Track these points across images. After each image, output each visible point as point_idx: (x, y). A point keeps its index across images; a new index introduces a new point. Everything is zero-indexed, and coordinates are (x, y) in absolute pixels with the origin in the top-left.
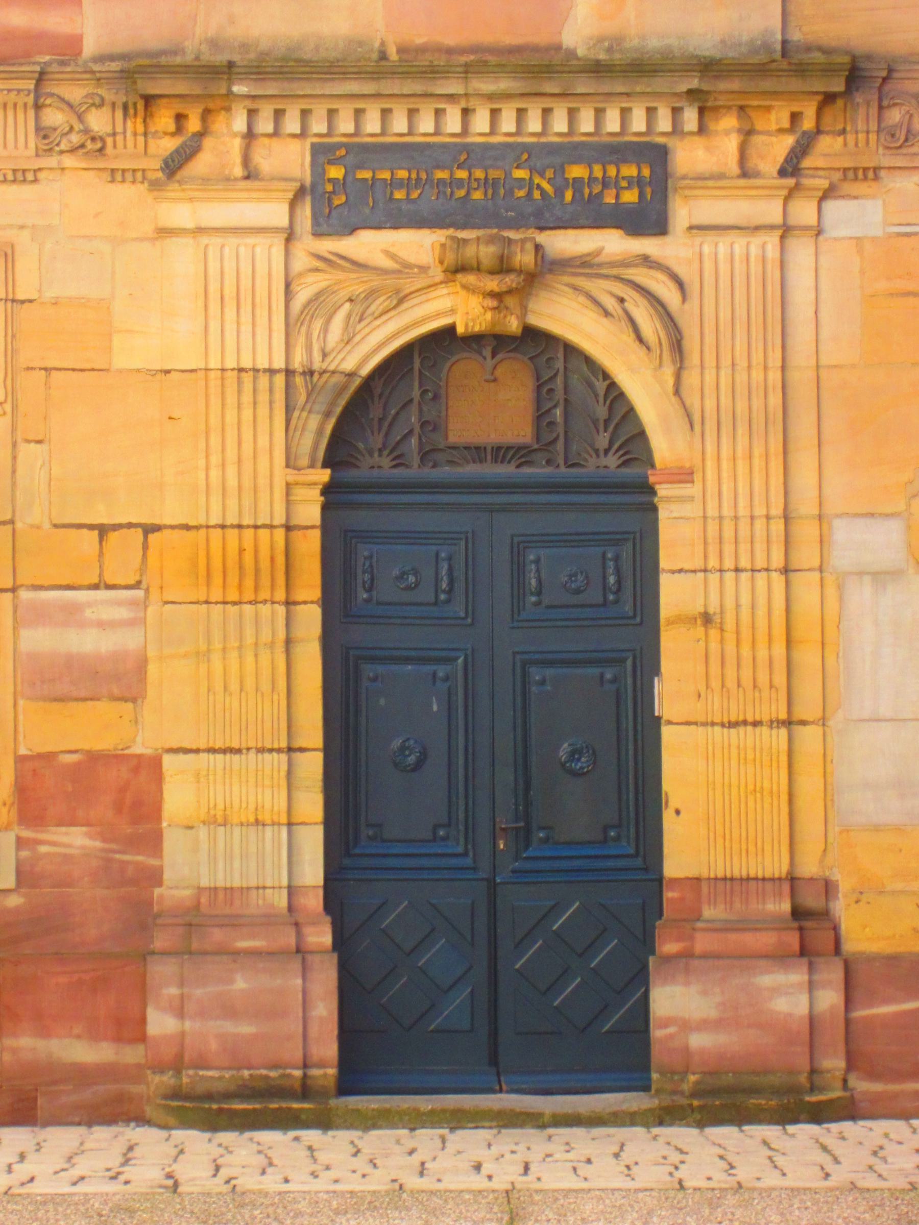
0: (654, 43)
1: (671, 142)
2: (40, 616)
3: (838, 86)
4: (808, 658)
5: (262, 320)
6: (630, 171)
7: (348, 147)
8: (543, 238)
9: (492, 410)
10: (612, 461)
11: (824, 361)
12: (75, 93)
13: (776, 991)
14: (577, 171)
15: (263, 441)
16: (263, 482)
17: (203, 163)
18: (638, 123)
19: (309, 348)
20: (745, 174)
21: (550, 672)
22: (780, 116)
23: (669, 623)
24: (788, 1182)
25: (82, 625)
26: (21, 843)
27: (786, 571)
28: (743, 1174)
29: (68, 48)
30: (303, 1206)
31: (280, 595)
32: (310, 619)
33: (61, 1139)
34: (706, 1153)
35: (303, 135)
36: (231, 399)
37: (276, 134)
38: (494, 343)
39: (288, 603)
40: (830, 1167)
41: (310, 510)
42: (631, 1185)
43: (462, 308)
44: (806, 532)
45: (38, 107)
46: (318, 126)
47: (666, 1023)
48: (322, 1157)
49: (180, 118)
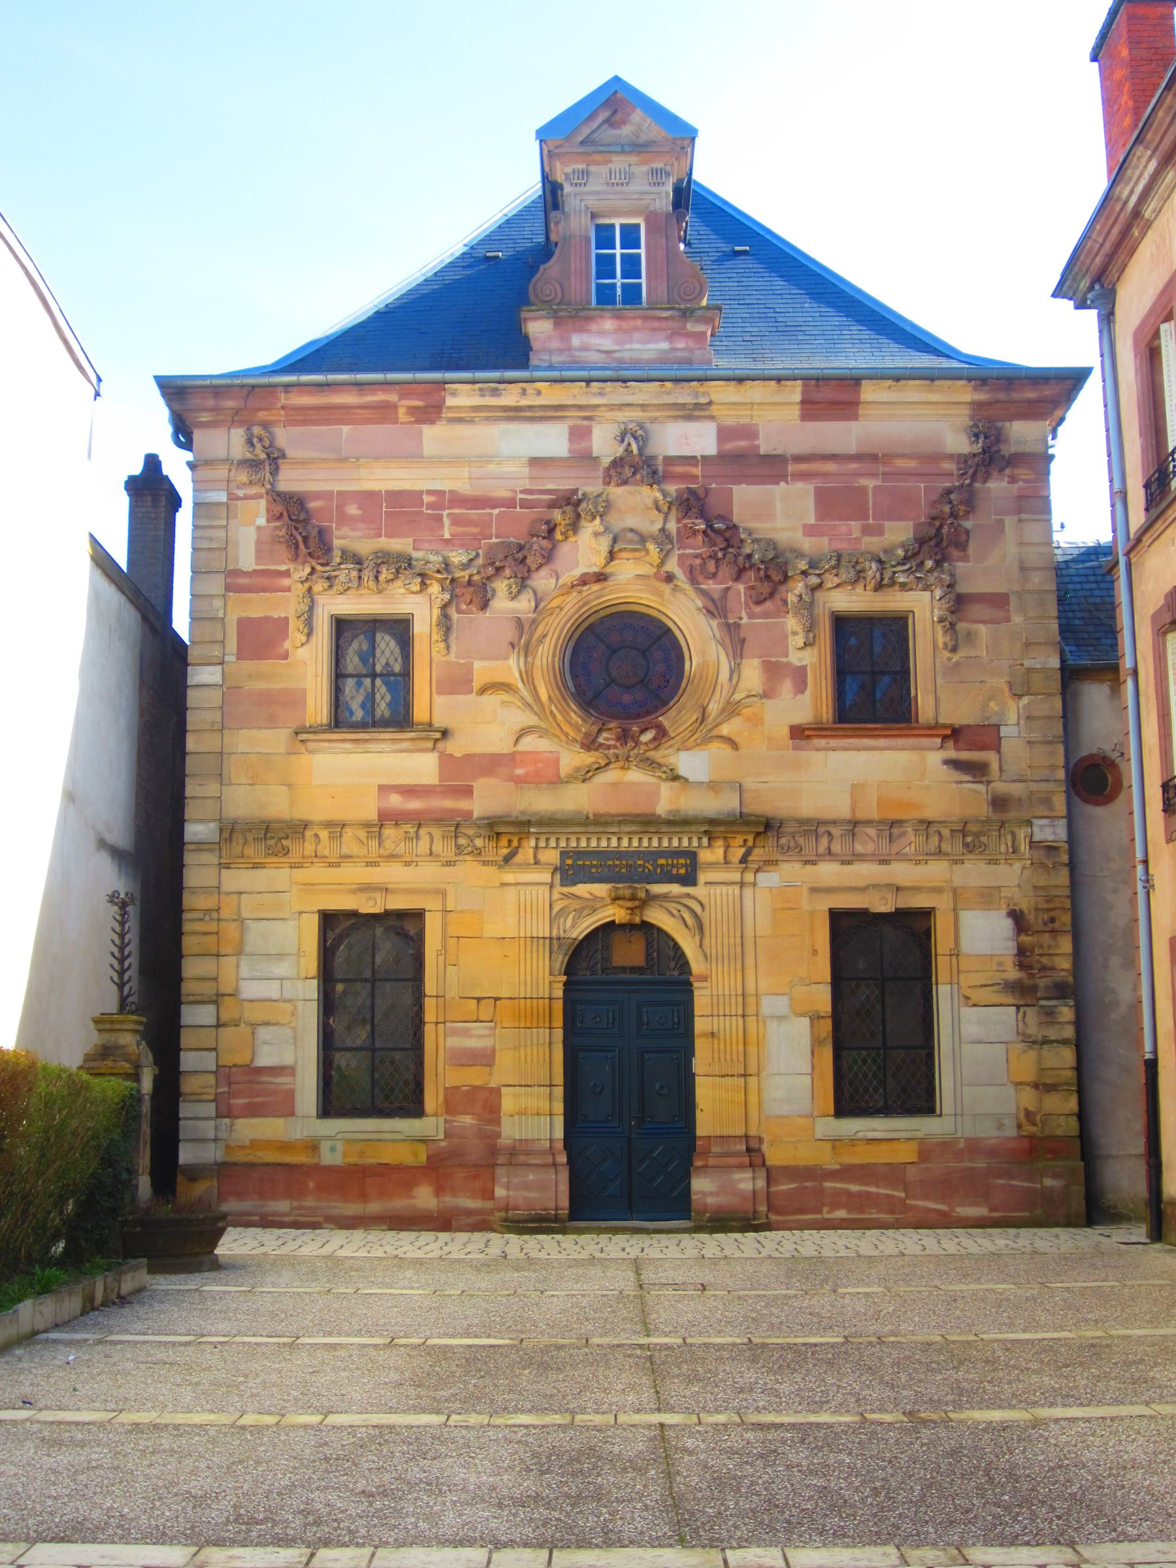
0: (691, 812)
1: (698, 850)
2: (455, 1032)
3: (761, 829)
4: (752, 1050)
5: (541, 919)
6: (682, 861)
7: (574, 852)
8: (649, 887)
9: (628, 953)
10: (676, 973)
11: (758, 934)
12: (470, 832)
13: (740, 1180)
14: (662, 861)
15: (541, 965)
16: (541, 981)
17: (518, 858)
18: (685, 843)
19: (559, 928)
20: (726, 863)
21: (652, 1055)
22: (739, 840)
23: (700, 1036)
24: (744, 1255)
25: (471, 1036)
26: (446, 1121)
27: (743, 1016)
28: (727, 1252)
29: (468, 815)
30: (555, 1265)
31: (547, 1025)
32: (559, 1034)
33: (463, 1236)
34: (713, 1244)
35: (556, 848)
36: (529, 949)
37: (546, 847)
38: (629, 927)
39: (550, 1028)
40: (761, 1249)
41: (559, 993)
42: (682, 1256)
43: (616, 914)
44: (751, 1000)
45: (456, 837)
46: (563, 844)
47: (698, 1193)
48: (563, 1245)
49: (510, 841)
